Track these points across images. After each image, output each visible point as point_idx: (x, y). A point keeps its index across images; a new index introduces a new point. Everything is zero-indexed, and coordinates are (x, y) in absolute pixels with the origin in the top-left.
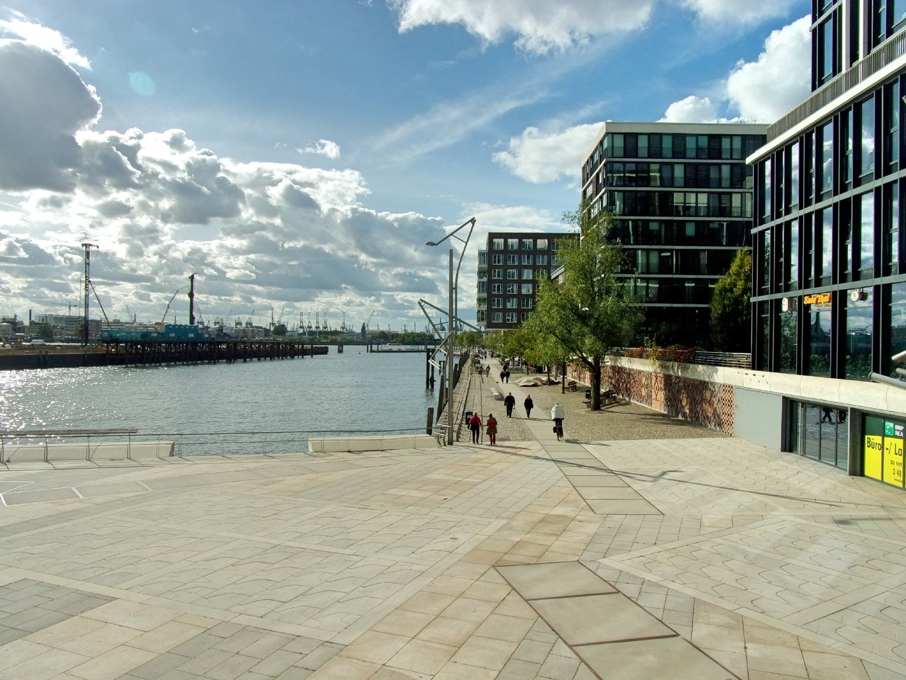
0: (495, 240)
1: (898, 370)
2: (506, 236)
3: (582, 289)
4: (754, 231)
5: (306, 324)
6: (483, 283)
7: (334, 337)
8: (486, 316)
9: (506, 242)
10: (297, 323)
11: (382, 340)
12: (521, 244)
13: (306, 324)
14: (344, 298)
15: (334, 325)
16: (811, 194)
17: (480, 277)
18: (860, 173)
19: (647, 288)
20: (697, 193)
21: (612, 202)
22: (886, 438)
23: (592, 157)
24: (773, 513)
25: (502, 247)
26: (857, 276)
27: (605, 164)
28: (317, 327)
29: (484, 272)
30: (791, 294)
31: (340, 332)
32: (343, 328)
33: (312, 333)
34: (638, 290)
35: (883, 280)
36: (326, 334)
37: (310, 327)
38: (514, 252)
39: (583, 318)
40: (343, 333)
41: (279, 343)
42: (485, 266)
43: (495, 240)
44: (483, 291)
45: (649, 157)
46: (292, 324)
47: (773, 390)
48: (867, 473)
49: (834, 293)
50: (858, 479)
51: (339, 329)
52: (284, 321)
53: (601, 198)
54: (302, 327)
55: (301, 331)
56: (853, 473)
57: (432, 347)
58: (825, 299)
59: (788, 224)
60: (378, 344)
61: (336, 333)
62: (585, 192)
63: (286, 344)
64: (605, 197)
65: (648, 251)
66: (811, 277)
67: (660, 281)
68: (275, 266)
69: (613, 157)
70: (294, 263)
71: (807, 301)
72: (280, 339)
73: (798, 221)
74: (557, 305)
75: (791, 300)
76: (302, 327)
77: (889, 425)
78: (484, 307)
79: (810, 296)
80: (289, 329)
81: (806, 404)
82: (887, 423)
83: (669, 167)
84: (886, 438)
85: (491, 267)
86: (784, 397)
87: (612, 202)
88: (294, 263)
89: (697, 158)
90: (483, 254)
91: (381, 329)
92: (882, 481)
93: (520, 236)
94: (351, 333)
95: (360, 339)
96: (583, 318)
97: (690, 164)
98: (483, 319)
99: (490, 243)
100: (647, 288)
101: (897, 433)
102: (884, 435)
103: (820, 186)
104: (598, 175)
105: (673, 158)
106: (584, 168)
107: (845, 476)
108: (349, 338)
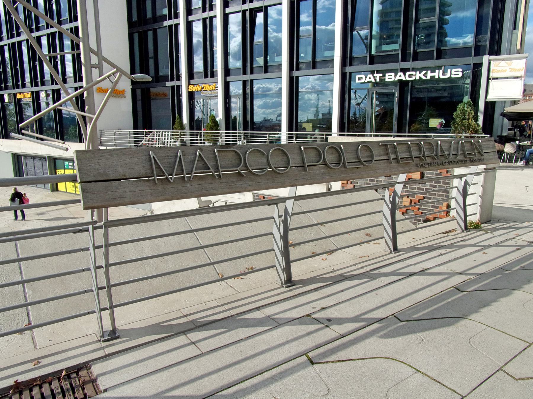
1: (23, 131)
4: (166, 23)
8: (481, 161)
16: (13, 31)
18: (39, 24)
24: (4, 217)
26: (43, 84)
30: (9, 91)
35: (35, 89)
47: (5, 150)
48: (59, 189)
49: (32, 92)
50: (55, 193)
56: (53, 190)
58: (29, 95)
59: (20, 43)
66: (19, 83)
71: (19, 96)
73: (201, 21)
75: (9, 95)
77: (66, 163)
79: (20, 93)
81: (26, 156)
82: (65, 162)
86: (12, 154)
92: (66, 192)
101: (70, 167)
102: (65, 169)
107: (49, 192)
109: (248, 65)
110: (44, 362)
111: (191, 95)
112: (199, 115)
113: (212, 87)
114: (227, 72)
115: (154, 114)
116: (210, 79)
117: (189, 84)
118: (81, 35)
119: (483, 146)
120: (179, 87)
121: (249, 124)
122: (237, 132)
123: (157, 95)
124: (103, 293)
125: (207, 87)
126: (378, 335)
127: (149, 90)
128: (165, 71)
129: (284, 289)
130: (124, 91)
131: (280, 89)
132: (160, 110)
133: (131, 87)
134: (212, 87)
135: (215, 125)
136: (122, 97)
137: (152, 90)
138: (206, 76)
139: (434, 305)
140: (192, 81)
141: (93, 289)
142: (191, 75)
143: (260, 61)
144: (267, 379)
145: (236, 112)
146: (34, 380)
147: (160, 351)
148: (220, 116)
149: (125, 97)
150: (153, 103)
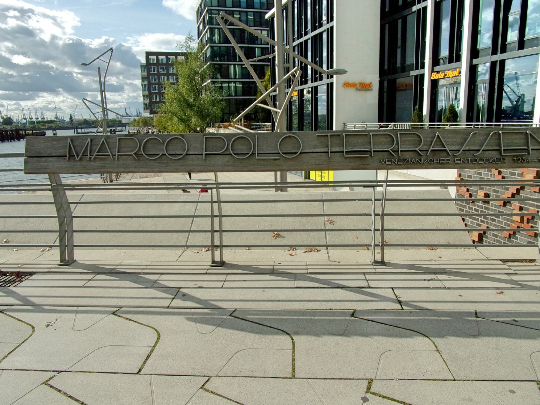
0: (150, 57)
2: (157, 54)
3: (188, 89)
5: (28, 117)
6: (145, 85)
7: (50, 125)
9: (157, 58)
10: (21, 117)
11: (85, 126)
12: (168, 59)
13: (28, 117)
14: (61, 98)
15: (50, 116)
17: (143, 81)
19: (229, 86)
20: (261, 30)
21: (212, 35)
22: (210, 204)
23: (201, 5)
25: (155, 62)
27: (207, 11)
28: (37, 118)
29: (145, 78)
31: (54, 121)
32: (57, 118)
33: (33, 123)
34: (237, 89)
36: (44, 122)
37: (37, 118)
38: (163, 64)
39: (190, 106)
40: (57, 122)
41: (7, 131)
42: (145, 74)
43: (150, 57)
44: (145, 90)
45: (233, 7)
46: (16, 116)
51: (53, 119)
52: (10, 114)
53: (206, 32)
54: (25, 119)
55: (25, 121)
57: (113, 129)
60: (82, 128)
61: (51, 122)
62: (199, 27)
63: (12, 131)
64: (209, 31)
65: (234, 65)
67: (243, 83)
68: (12, 76)
69: (211, 6)
70: (26, 74)
72: (9, 128)
74: (175, 99)
76: (25, 119)
78: (147, 101)
80: (15, 120)
83: (245, 14)
84: (210, 204)
85: (149, 75)
87: (212, 35)
88: (26, 74)
89: (261, 9)
90: (143, 66)
91: (85, 117)
93: (167, 54)
94: (63, 121)
95: (69, 125)
96: (190, 106)
97: (256, 12)
98: (147, 109)
99: (148, 59)
100: (229, 86)
103: (306, 27)
104: (204, 17)
105: (247, 8)
106: (197, 12)
108: (61, 125)
109: (499, 43)
110: (25, 266)
111: (434, 84)
112: (441, 105)
113: (456, 73)
114: (474, 53)
115: (398, 105)
116: (454, 65)
117: (433, 71)
118: (276, 40)
119: (77, 210)
120: (422, 76)
121: (495, 112)
122: (480, 123)
123: (406, 85)
124: (378, 234)
125: (450, 74)
126: (185, 316)
127: (395, 80)
128: (411, 60)
129: (372, 267)
130: (371, 83)
131: (268, 105)
132: (404, 101)
133: (379, 79)
134: (456, 73)
135: (453, 116)
136: (368, 90)
137: (398, 81)
138: (451, 61)
139: (532, 321)
140: (436, 68)
141: (372, 229)
142: (436, 61)
143: (513, 36)
144: (106, 311)
145: (482, 99)
146: (8, 272)
147: (192, 279)
148: (461, 105)
149: (372, 90)
150: (398, 94)
